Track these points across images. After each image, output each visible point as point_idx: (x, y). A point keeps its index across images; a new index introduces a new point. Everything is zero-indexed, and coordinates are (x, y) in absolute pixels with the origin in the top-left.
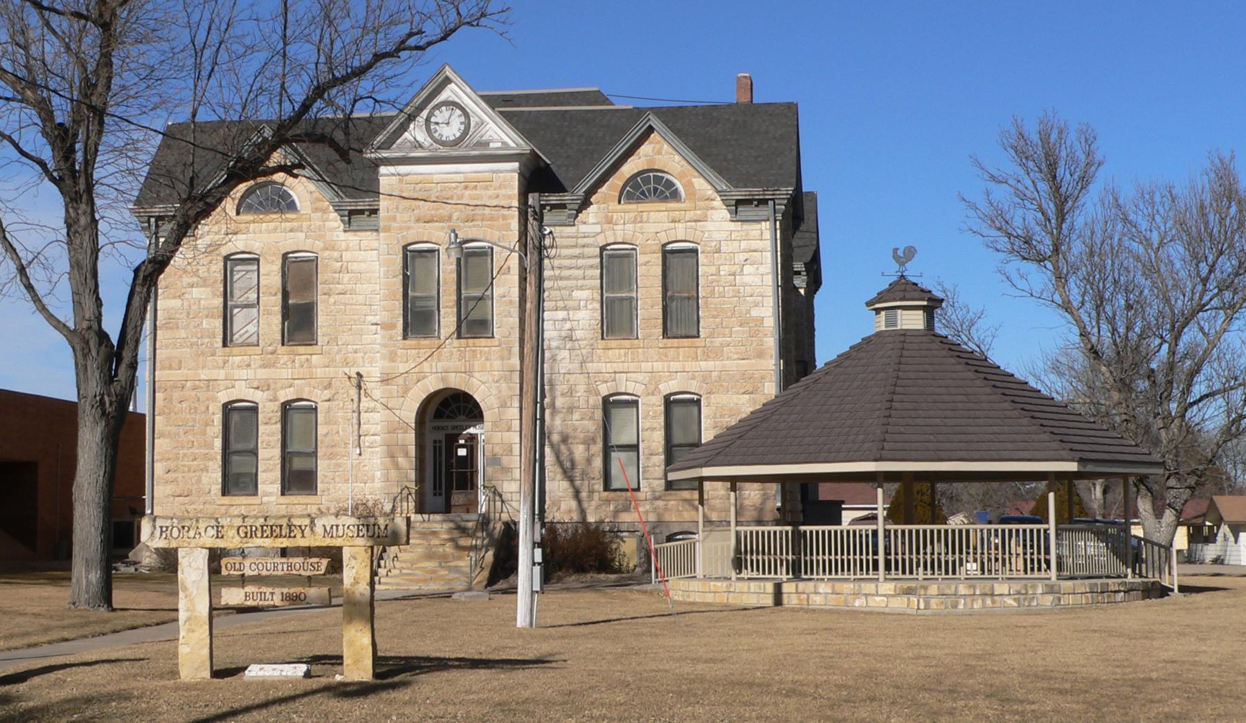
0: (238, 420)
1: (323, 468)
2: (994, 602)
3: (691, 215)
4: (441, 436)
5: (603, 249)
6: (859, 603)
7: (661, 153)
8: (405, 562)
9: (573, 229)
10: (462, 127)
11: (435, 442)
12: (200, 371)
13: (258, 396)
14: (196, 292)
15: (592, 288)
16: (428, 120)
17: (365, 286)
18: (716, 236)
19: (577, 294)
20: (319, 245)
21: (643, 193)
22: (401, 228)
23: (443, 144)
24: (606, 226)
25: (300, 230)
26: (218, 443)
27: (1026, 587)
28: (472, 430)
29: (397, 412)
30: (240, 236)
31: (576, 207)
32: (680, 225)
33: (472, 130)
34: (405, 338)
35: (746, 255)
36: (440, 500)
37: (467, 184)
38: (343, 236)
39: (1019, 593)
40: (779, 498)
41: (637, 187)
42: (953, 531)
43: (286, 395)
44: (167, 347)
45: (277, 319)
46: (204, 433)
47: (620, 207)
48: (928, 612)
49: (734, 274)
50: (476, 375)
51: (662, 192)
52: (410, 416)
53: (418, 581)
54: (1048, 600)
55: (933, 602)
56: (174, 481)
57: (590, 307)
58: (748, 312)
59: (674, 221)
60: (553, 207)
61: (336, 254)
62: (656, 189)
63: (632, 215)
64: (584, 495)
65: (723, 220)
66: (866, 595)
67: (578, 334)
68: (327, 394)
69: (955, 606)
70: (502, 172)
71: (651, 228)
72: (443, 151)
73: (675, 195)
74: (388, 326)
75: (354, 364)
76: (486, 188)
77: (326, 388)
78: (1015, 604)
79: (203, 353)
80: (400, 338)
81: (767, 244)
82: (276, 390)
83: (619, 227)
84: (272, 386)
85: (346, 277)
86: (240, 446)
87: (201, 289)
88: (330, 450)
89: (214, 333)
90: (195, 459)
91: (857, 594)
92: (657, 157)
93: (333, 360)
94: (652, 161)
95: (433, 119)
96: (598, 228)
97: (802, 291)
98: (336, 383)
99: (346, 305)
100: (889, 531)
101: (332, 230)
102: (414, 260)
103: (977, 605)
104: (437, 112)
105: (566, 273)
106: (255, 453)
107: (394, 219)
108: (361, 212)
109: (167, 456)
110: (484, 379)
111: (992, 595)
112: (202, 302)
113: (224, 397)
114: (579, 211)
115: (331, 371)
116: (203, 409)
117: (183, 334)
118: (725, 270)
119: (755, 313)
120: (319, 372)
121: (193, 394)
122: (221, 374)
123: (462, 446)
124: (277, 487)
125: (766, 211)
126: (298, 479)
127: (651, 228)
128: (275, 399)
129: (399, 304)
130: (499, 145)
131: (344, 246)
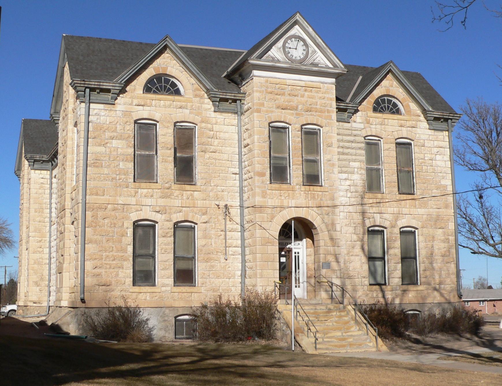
0: (144, 232)
3: (409, 123)
9: (346, 125)
10: (305, 53)
12: (118, 198)
14: (115, 143)
16: (284, 46)
17: (228, 148)
18: (423, 137)
19: (352, 164)
20: (197, 119)
22: (267, 111)
23: (292, 61)
24: (367, 125)
30: (146, 108)
32: (404, 129)
33: (310, 55)
35: (438, 149)
37: (306, 88)
38: (213, 114)
43: (178, 217)
44: (94, 179)
45: (171, 166)
46: (120, 241)
49: (432, 160)
51: (169, 89)
61: (209, 126)
62: (392, 109)
63: (380, 120)
68: (205, 218)
70: (326, 83)
71: (390, 129)
72: (295, 66)
73: (398, 112)
75: (222, 198)
76: (317, 92)
77: (204, 214)
82: (170, 213)
83: (373, 126)
84: (168, 211)
85: (216, 142)
86: (143, 252)
87: (119, 141)
89: (127, 172)
90: (114, 260)
92: (391, 88)
94: (388, 90)
95: (287, 45)
96: (362, 126)
99: (216, 159)
101: (206, 110)
104: (289, 41)
106: (153, 256)
107: (263, 105)
108: (226, 100)
109: (94, 257)
112: (119, 150)
113: (134, 217)
116: (120, 224)
119: (443, 182)
120: (200, 203)
121: (113, 213)
122: (133, 201)
126: (184, 276)
129: (267, 160)
131: (214, 121)
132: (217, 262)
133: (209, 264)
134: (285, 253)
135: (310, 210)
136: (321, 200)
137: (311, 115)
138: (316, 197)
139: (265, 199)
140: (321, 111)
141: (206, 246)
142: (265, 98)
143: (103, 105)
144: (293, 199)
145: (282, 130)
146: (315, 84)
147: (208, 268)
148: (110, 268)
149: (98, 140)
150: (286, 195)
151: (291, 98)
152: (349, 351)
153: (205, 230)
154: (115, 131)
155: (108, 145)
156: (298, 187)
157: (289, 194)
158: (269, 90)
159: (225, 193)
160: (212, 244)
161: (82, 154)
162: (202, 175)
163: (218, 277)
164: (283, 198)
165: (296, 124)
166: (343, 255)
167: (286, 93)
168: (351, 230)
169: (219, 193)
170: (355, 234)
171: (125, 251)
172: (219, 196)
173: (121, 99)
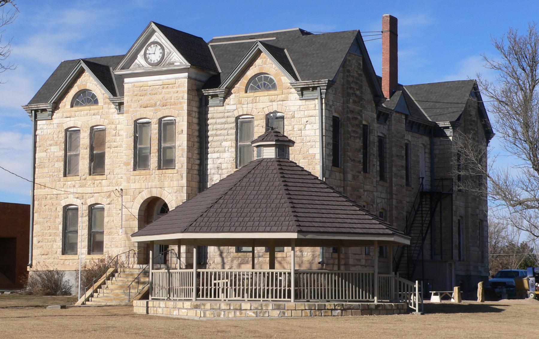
0: (69, 214)
1: (106, 239)
2: (241, 314)
5: (237, 118)
6: (175, 313)
7: (266, 64)
10: (161, 55)
13: (78, 202)
15: (231, 140)
16: (145, 54)
18: (292, 109)
21: (258, 86)
23: (152, 65)
24: (239, 106)
25: (98, 114)
26: (61, 227)
27: (261, 305)
29: (130, 210)
30: (72, 119)
31: (223, 96)
33: (165, 56)
34: (134, 170)
35: (307, 119)
37: (164, 86)
38: (117, 116)
39: (257, 309)
40: (321, 256)
41: (255, 83)
42: (211, 273)
46: (55, 222)
47: (246, 94)
48: (205, 319)
49: (301, 130)
50: (166, 189)
52: (135, 211)
53: (111, 300)
54: (276, 313)
55: (208, 313)
56: (41, 247)
57: (230, 151)
58: (308, 151)
59: (271, 101)
60: (213, 96)
61: (113, 126)
62: (265, 84)
63: (251, 99)
64: (224, 255)
65: (296, 99)
66: (179, 308)
67: (224, 166)
68: (108, 201)
69: (219, 315)
70: (179, 78)
73: (274, 87)
74: (127, 164)
78: (254, 315)
79: (55, 180)
80: (132, 170)
81: (317, 112)
85: (118, 138)
91: (174, 308)
93: (111, 183)
95: (148, 52)
96: (234, 107)
97: (451, 138)
99: (118, 153)
100: (199, 273)
101: (112, 114)
102: (140, 128)
103: (231, 315)
105: (219, 132)
107: (130, 106)
109: (38, 234)
110: (170, 191)
111: (241, 309)
112: (55, 154)
114: (225, 98)
116: (54, 209)
117: (46, 170)
118: (296, 127)
119: (311, 151)
121: (50, 201)
124: (85, 250)
125: (317, 93)
127: (260, 105)
128: (86, 204)
130: (179, 64)
137: (167, 109)
140: (175, 104)
142: (132, 101)
143: (45, 121)
145: (146, 125)
146: (170, 81)
148: (48, 242)
149: (42, 148)
151: (151, 96)
154: (53, 139)
155: (48, 151)
158: (136, 93)
160: (113, 221)
163: (117, 247)
165: (154, 118)
167: (148, 93)
171: (58, 229)
173: (57, 114)
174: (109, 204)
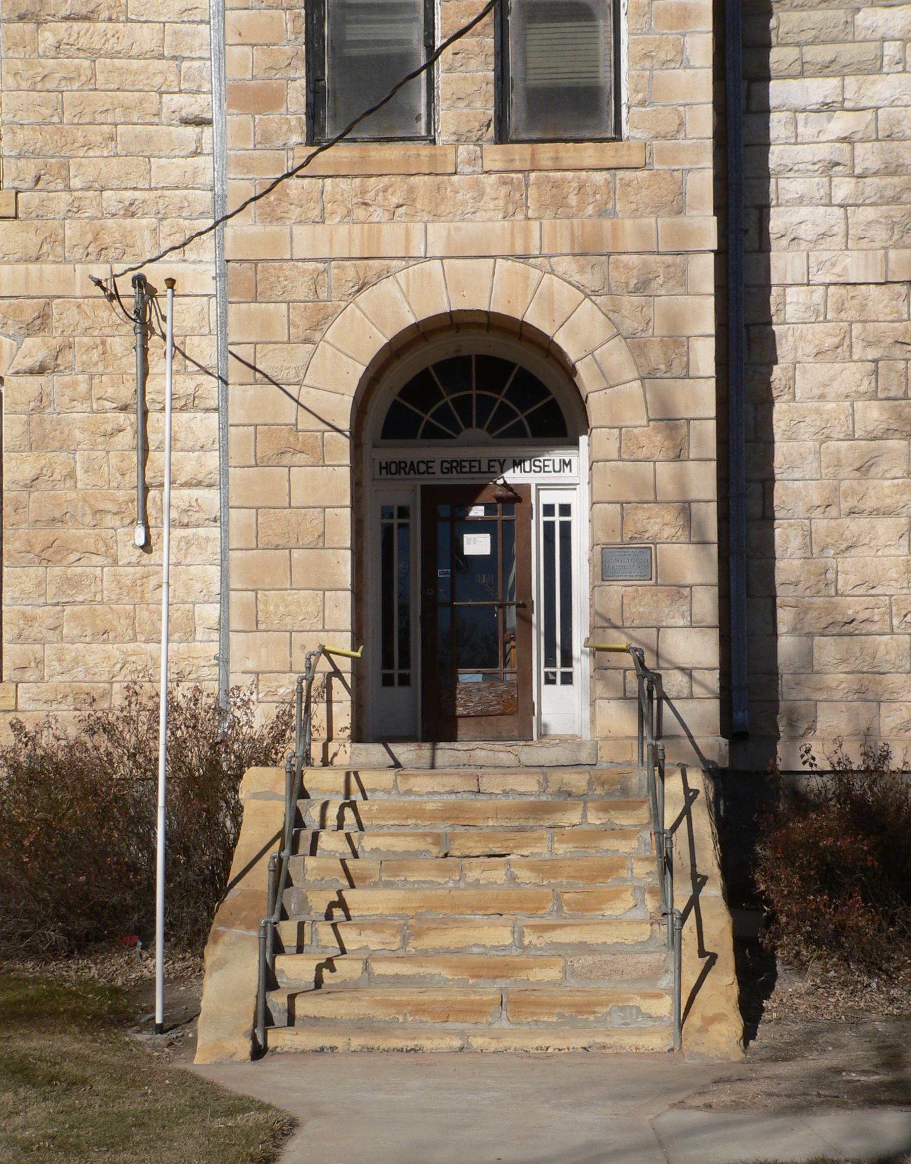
4: (405, 493)
8: (377, 924)
11: (386, 512)
28: (512, 477)
36: (407, 700)
68: (35, 349)
74: (252, 98)
88: (42, 536)
93: (55, 239)
98: (64, 315)
99: (94, 54)
115: (47, 276)
123: (478, 527)
132: (96, 559)
133: (57, 570)
134: (489, 509)
135: (535, 274)
136: (602, 213)
138: (573, 200)
139: (275, 228)
141: (40, 484)
144: (437, 217)
147: (52, 589)
150: (394, 200)
152: (477, 1042)
153: (39, 409)
156: (464, 151)
157: (411, 190)
159: (144, 222)
160: (71, 475)
161: (709, 260)
162: (21, 135)
163: (104, 634)
164: (378, 214)
166: (801, 510)
168: (851, 375)
169: (110, 222)
170: (874, 397)
172: (106, 239)
174: (41, 370)
